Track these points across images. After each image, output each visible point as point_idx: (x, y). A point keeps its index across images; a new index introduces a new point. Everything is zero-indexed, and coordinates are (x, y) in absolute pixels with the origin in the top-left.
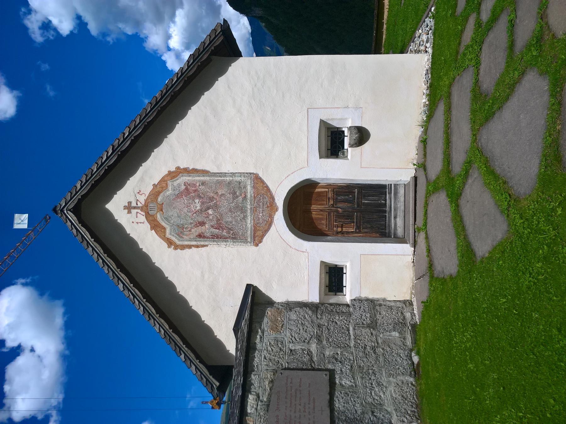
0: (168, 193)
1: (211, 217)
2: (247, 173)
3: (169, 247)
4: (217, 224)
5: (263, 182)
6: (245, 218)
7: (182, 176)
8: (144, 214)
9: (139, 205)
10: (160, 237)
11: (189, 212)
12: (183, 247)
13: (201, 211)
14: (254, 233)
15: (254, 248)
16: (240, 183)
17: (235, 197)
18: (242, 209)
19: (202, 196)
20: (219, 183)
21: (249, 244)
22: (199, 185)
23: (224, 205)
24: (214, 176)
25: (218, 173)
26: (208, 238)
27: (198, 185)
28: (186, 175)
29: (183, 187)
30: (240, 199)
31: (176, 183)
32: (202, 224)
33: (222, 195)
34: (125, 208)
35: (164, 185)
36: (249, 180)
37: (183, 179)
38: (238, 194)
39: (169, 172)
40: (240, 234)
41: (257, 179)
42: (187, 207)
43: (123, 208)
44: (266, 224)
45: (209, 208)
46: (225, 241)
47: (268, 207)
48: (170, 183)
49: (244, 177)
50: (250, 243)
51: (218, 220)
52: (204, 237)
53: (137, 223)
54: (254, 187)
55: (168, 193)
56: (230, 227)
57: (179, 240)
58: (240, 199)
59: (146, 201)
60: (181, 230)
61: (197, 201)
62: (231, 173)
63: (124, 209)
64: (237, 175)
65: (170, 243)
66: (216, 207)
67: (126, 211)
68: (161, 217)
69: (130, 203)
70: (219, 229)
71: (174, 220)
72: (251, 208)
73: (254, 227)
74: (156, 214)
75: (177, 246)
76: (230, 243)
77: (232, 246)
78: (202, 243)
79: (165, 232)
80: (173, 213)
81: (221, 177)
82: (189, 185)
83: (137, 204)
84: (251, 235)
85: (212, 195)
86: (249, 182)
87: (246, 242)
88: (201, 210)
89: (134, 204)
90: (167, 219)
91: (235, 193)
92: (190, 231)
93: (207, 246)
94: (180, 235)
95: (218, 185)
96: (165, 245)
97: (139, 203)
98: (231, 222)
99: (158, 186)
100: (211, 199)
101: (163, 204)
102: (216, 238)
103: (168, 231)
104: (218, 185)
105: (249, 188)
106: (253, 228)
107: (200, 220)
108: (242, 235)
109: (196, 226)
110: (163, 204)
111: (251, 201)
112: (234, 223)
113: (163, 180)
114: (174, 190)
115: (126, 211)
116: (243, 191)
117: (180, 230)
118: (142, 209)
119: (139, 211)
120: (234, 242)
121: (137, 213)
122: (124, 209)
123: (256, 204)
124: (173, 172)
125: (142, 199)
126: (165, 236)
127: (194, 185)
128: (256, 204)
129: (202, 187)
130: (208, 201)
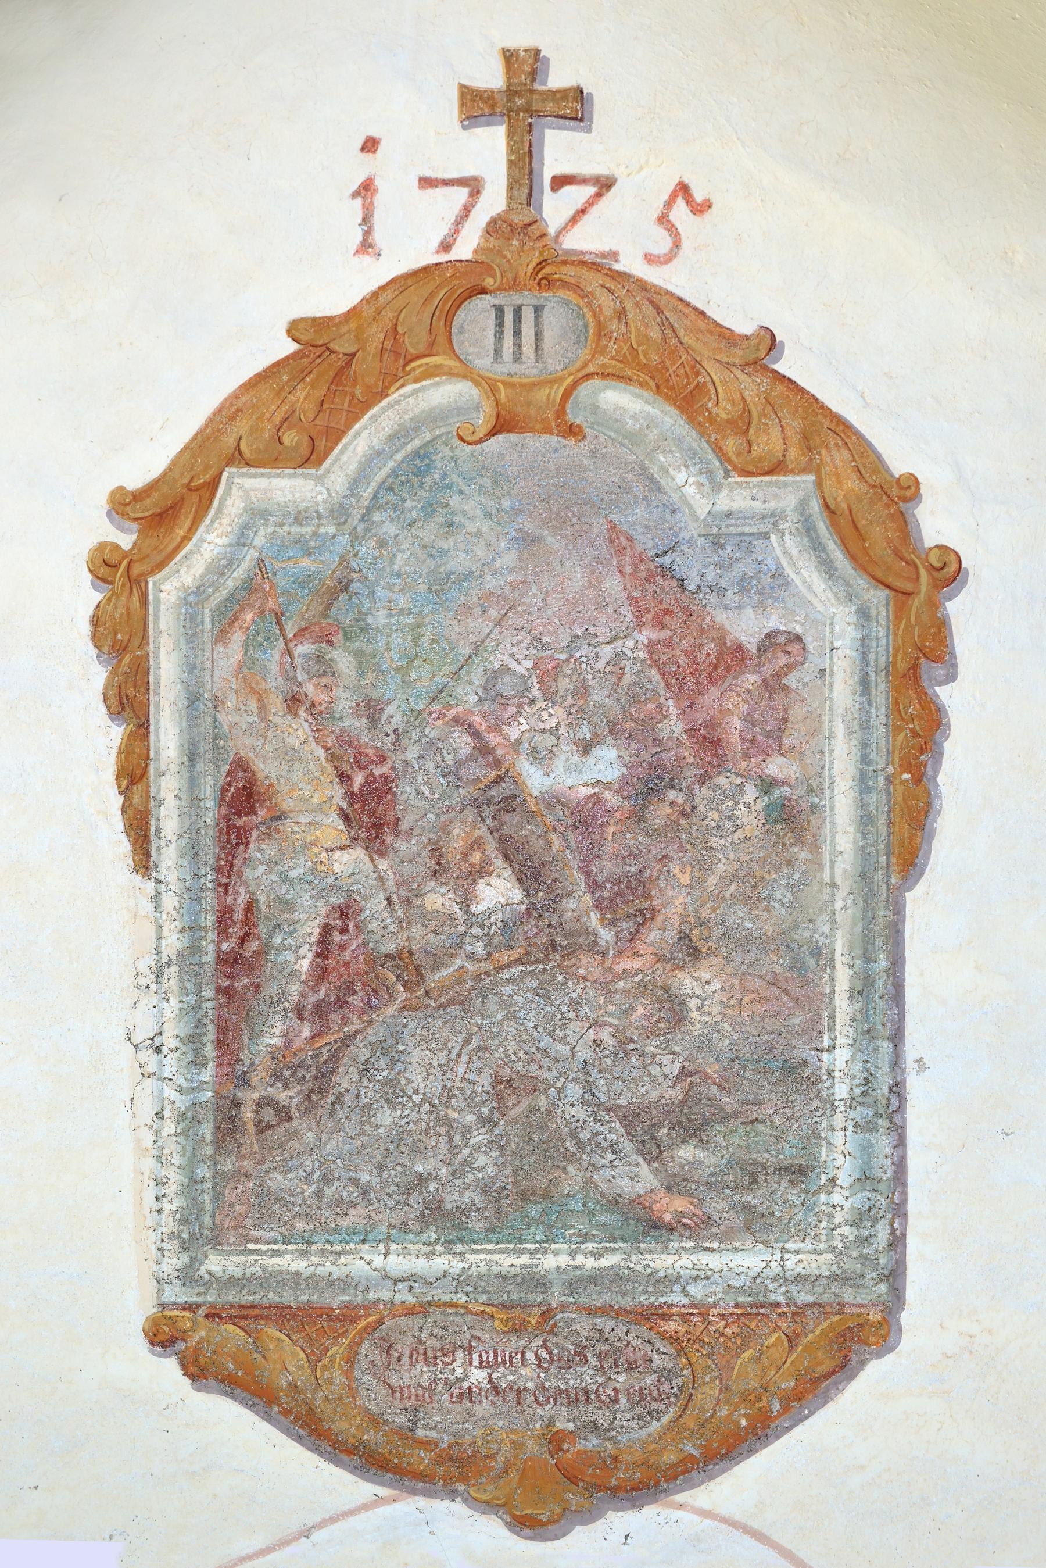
0: (684, 482)
1: (438, 899)
2: (897, 1242)
3: (123, 504)
4: (377, 960)
5: (811, 1390)
6: (444, 1222)
7: (864, 614)
8: (464, 250)
9: (555, 208)
10: (228, 412)
11: (491, 693)
12: (121, 637)
13: (500, 801)
14: (281, 1314)
15: (136, 1307)
16: (798, 1173)
17: (651, 1130)
18: (525, 1195)
19: (659, 815)
20: (798, 969)
21: (170, 1265)
22: (767, 785)
23: (565, 1033)
24: (868, 916)
25: (897, 963)
26: (227, 870)
27: (775, 767)
28: (880, 655)
29: (747, 627)
30: (636, 1178)
31: (787, 550)
32: (370, 814)
33: (674, 1011)
34: (524, 66)
35: (769, 442)
36: (821, 1264)
37: (831, 616)
38: (687, 1153)
39: (909, 489)
40: (277, 1181)
41: (838, 1338)
42: (547, 675)
43: (521, 41)
44: (376, 1421)
45: (530, 874)
46: (193, 1040)
47: (556, 1440)
48: (791, 493)
49: (864, 1217)
50: (187, 1276)
51: (410, 967)
52: (233, 839)
53: (366, 189)
54: (754, 1311)
55: (684, 482)
56: (346, 1079)
57: (192, 601)
58: (636, 1178)
59: (599, 265)
60: (299, 611)
61: (607, 764)
62: (897, 1089)
63: (509, 57)
64: (883, 1143)
65: (164, 510)
66: (543, 942)
67: (492, 77)
68: (434, 417)
69: (575, 107)
70: (321, 974)
71: (401, 552)
72: (542, 1283)
73: (349, 1315)
74: (467, 373)
75: (136, 584)
76: (179, 1082)
77: (147, 1109)
78: (169, 821)
79: (272, 457)
80: (480, 543)
81: (862, 990)
82: (774, 686)
83: (560, 182)
84: (267, 1279)
85: (674, 902)
86: (807, 1258)
87: (196, 1234)
88: (509, 804)
89: (560, 149)
90: (414, 474)
91: (692, 1129)
92: (294, 701)
93: (144, 861)
94: (247, 604)
95: (777, 964)
96: (145, 464)
97: (576, 195)
98: (393, 1092)
99: (751, 387)
100: (630, 900)
101: (573, 431)
102: (230, 962)
103: (287, 488)
104: (777, 964)
105: (747, 1261)
106: (337, 1300)
107: (406, 791)
108: (264, 1194)
109: (345, 759)
110: (573, 431)
111: (616, 1278)
112: (386, 1117)
113: (821, 430)
114: (717, 543)
115: (492, 77)
116: (717, 1206)
117: (301, 611)
118: (516, 227)
119: (494, 201)
120: (189, 1120)
121: (474, 186)
122: (509, 57)
123: (583, 1325)
124: (904, 527)
125: (616, 233)
126: (236, 457)
127: (777, 735)
128: (583, 1325)
129: (749, 810)
130: (606, 867)
